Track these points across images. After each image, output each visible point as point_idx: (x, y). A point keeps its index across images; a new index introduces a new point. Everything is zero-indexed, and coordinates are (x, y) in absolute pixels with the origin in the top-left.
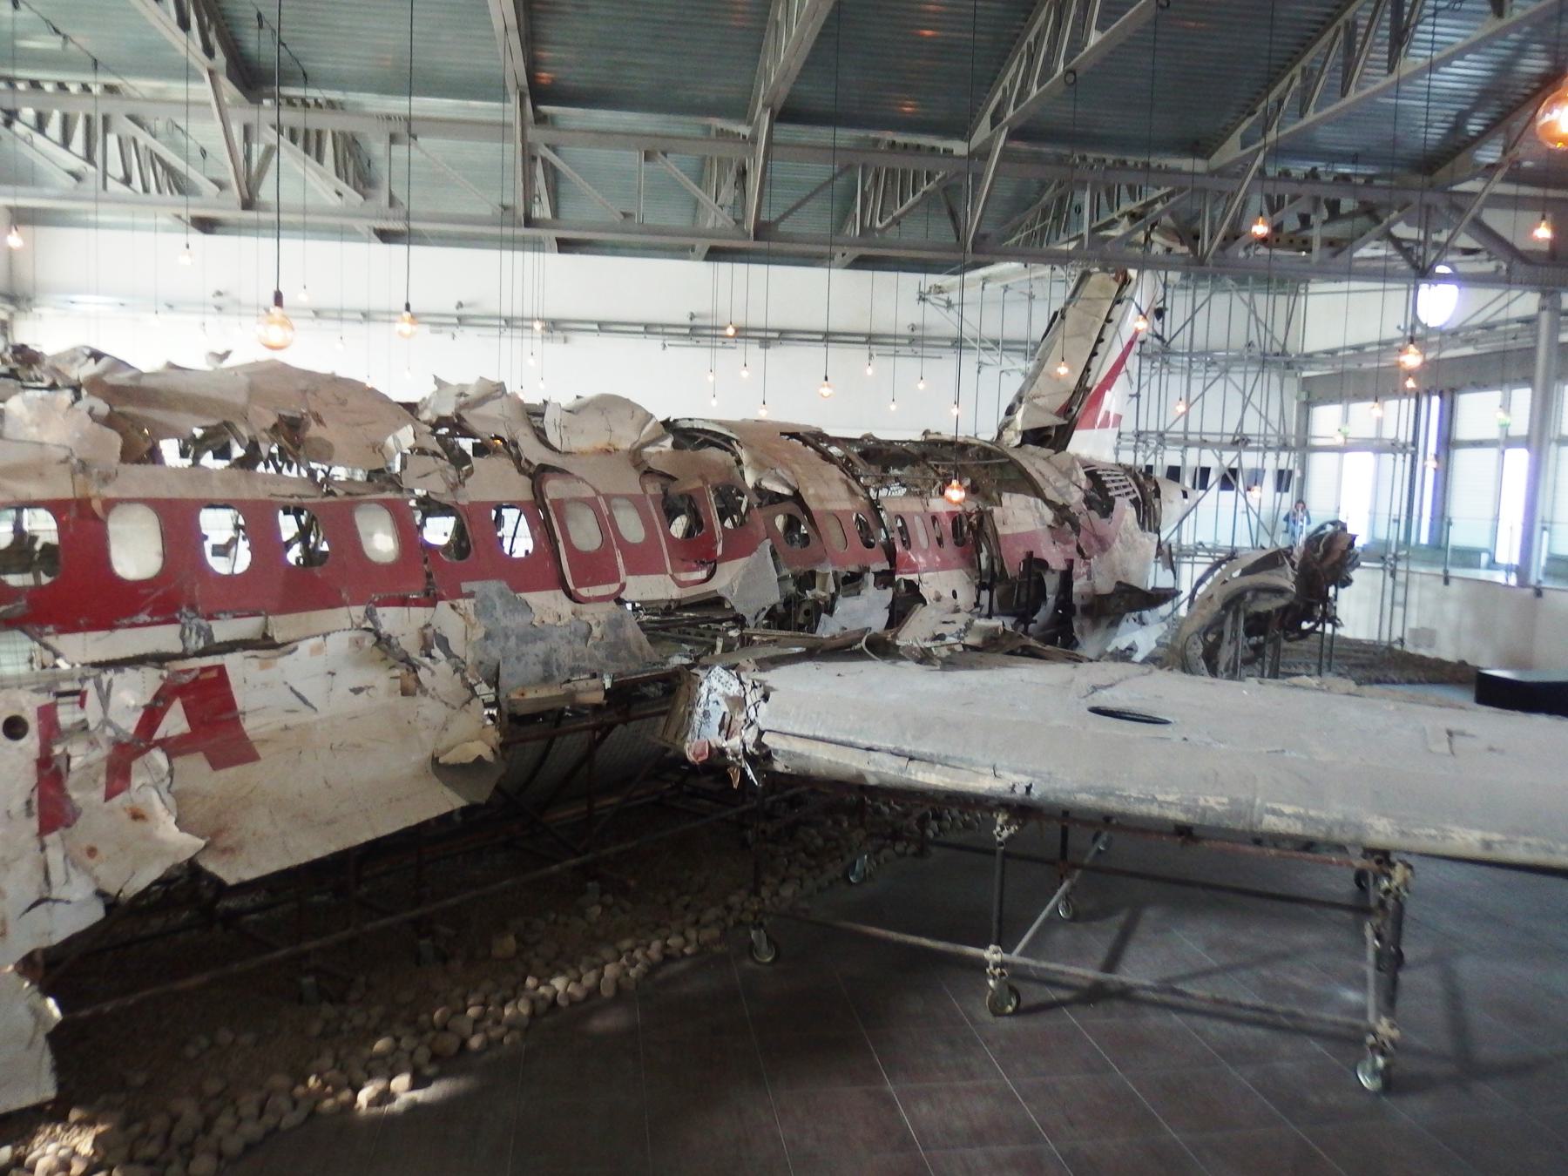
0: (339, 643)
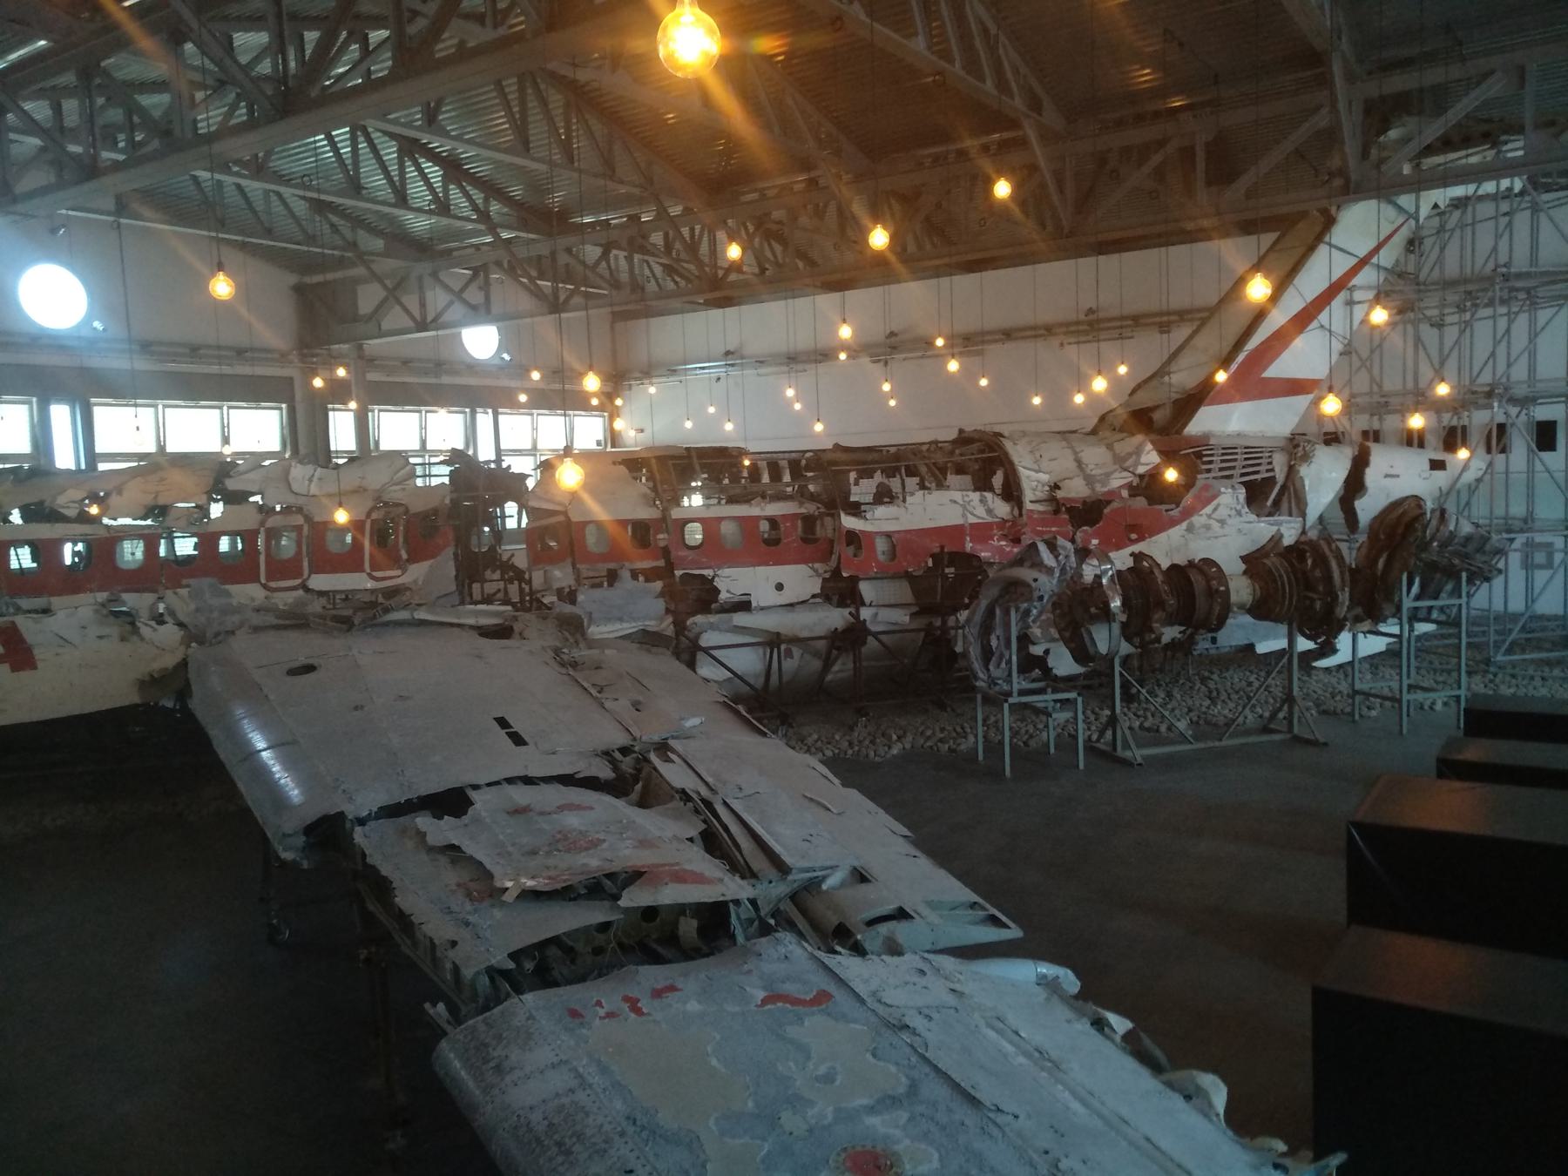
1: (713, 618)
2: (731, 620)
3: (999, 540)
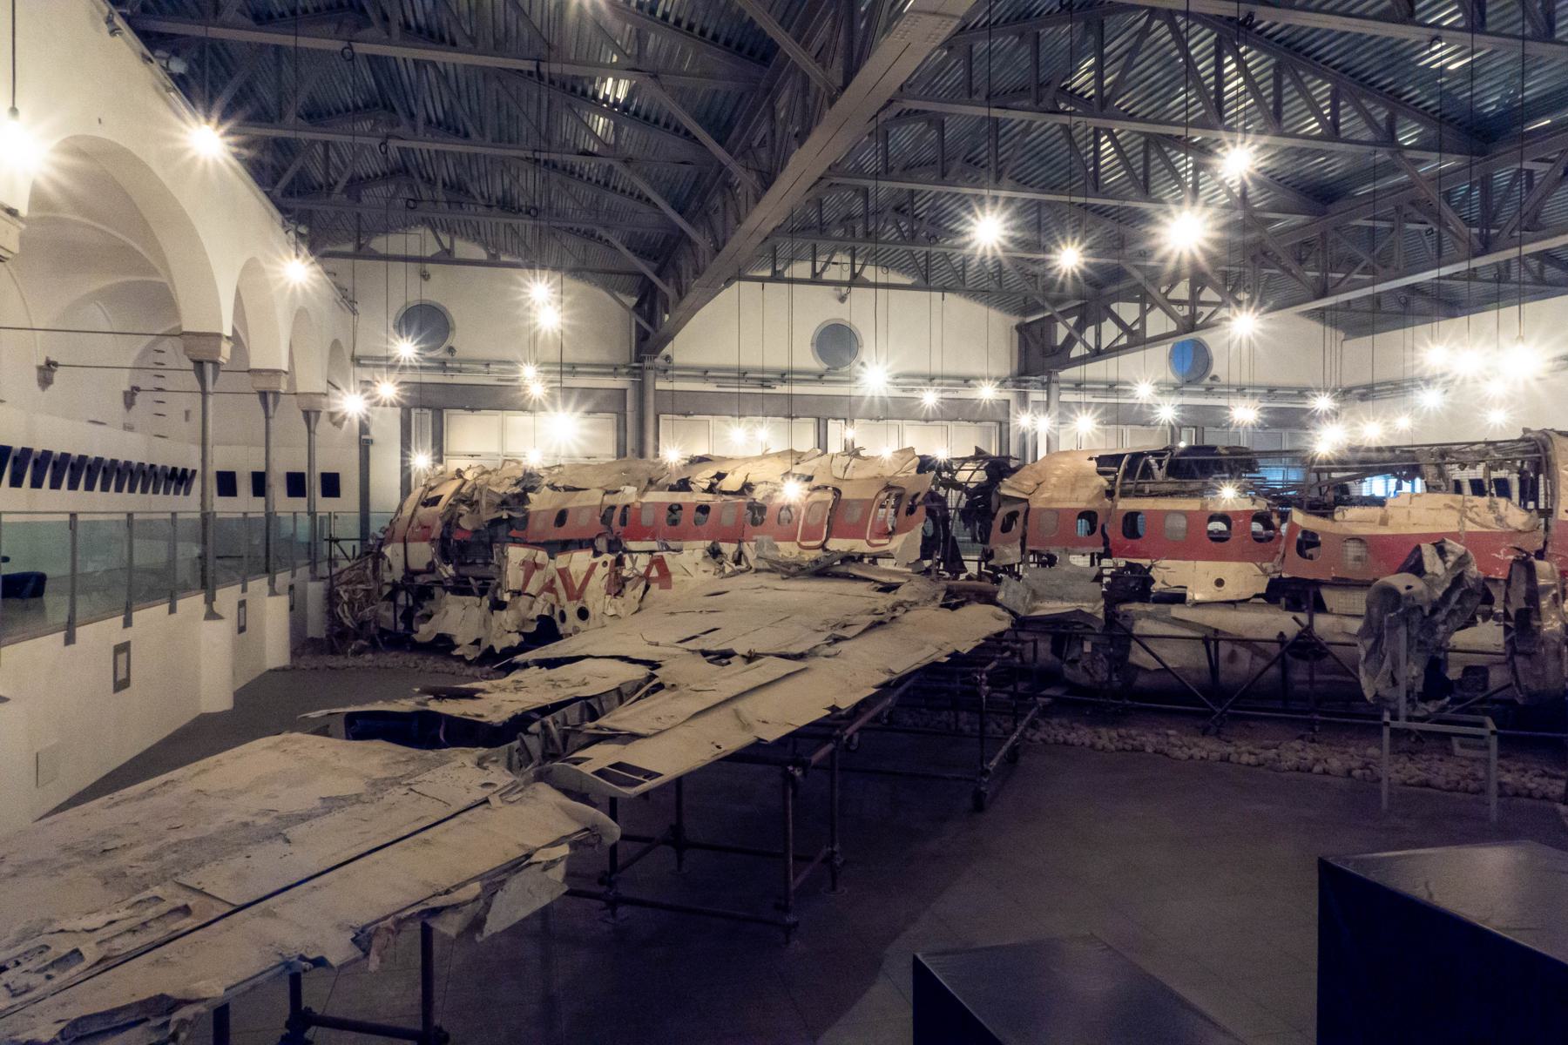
0: (699, 554)
1: (1150, 608)
2: (1169, 611)
3: (1506, 554)
